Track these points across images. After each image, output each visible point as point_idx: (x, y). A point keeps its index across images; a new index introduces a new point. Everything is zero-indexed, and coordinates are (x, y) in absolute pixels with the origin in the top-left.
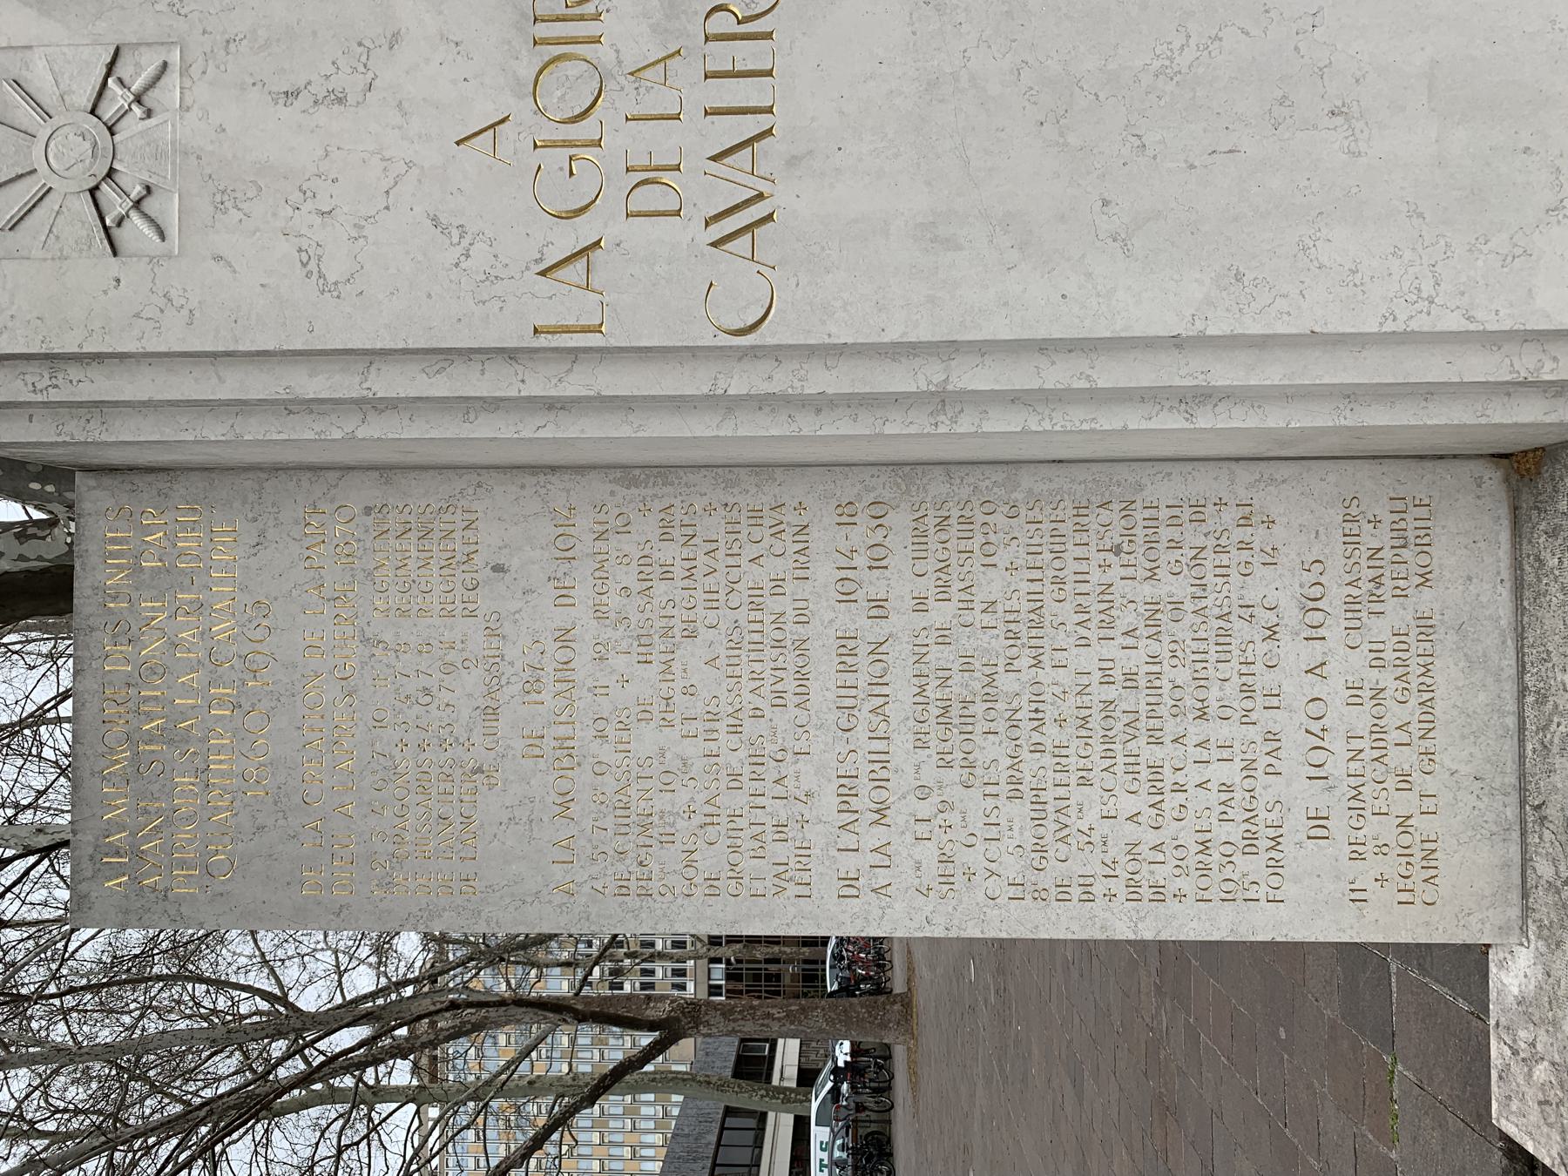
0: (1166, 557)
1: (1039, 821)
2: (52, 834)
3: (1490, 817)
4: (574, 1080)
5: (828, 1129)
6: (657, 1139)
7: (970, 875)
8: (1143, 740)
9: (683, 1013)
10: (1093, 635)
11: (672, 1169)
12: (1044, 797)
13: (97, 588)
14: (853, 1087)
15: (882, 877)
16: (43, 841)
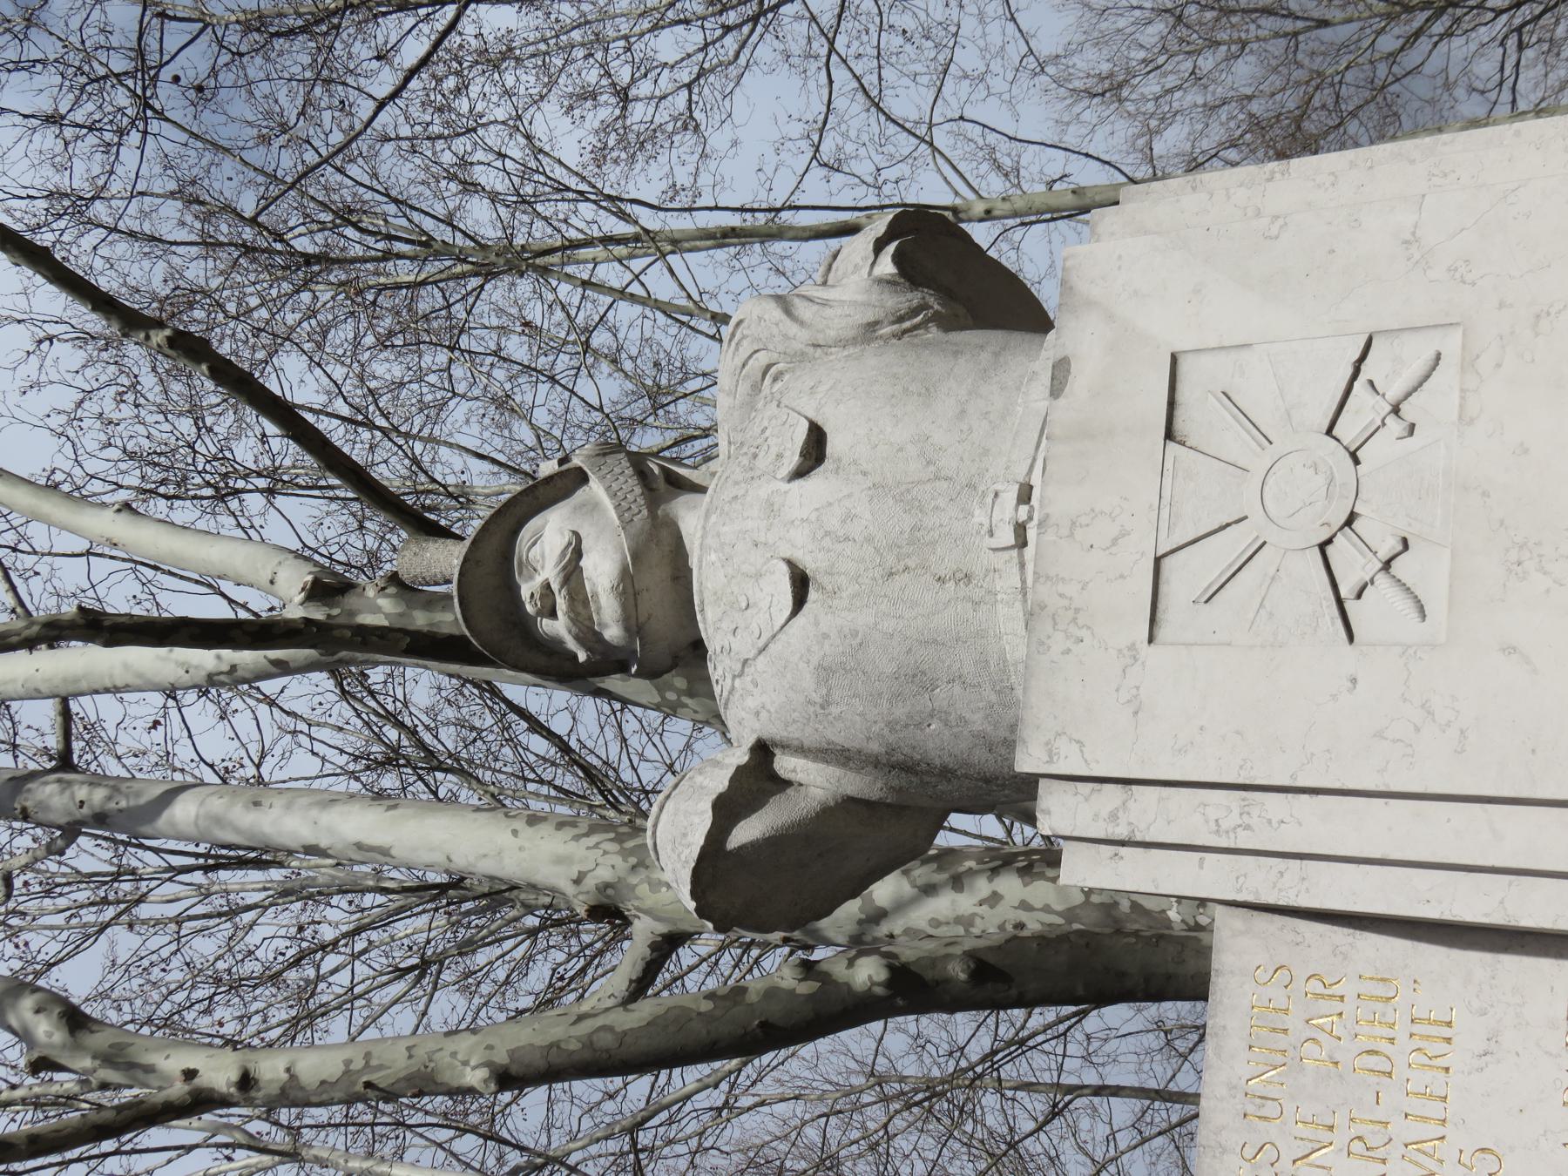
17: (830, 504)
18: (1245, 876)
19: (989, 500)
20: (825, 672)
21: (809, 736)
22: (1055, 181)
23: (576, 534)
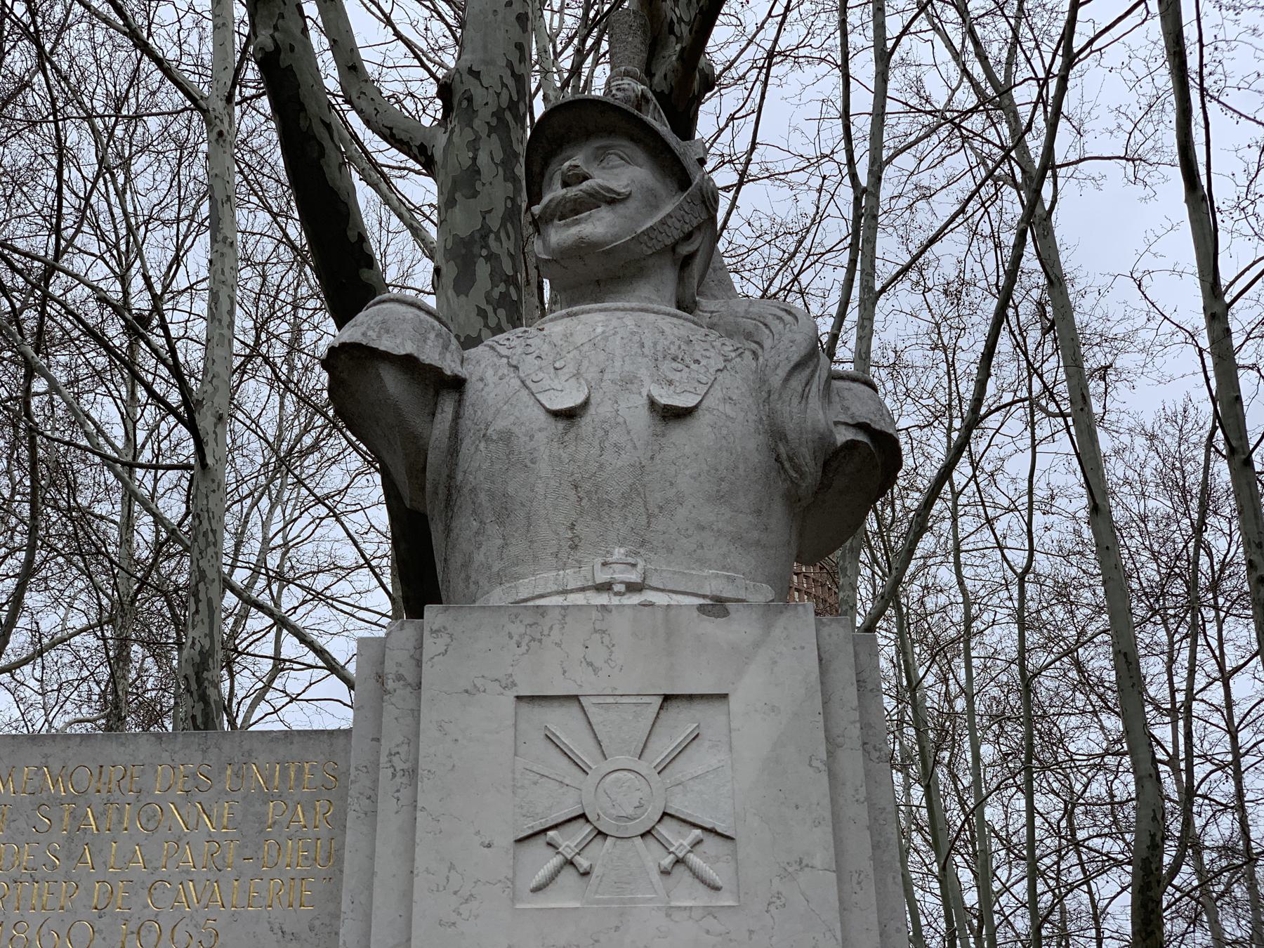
2: (215, 432)
13: (250, 755)
17: (629, 433)
18: (368, 772)
19: (630, 560)
20: (507, 437)
21: (466, 423)
22: (1259, 371)
23: (629, 196)
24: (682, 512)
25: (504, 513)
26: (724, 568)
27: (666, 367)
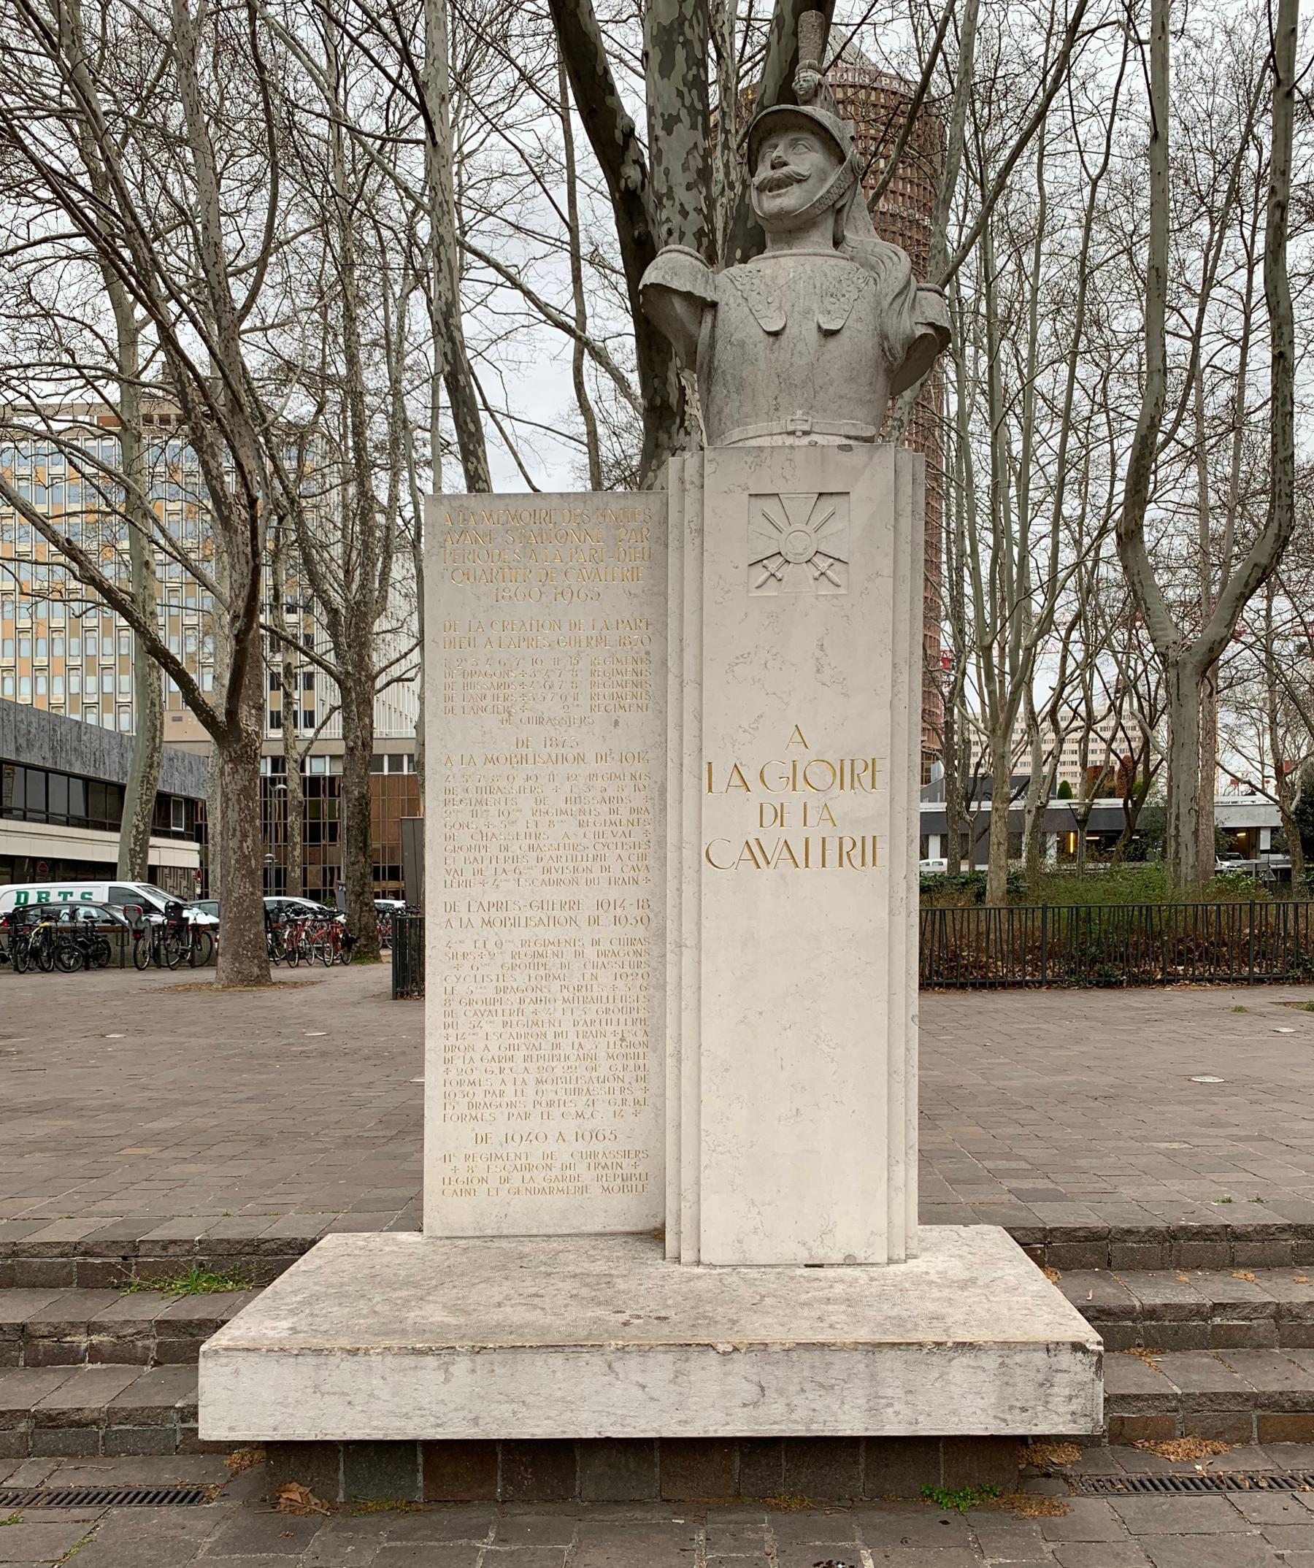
0: (619, 1063)
1: (485, 1002)
3: (487, 1221)
4: (151, 613)
5: (106, 900)
6: (58, 696)
7: (457, 967)
8: (526, 1053)
9: (246, 745)
10: (580, 1028)
11: (43, 723)
12: (498, 1004)
14: (160, 926)
15: (456, 924)
16: (432, 104)
20: (742, 344)
21: (719, 331)
24: (832, 389)
25: (740, 388)
26: (852, 418)
27: (828, 300)
